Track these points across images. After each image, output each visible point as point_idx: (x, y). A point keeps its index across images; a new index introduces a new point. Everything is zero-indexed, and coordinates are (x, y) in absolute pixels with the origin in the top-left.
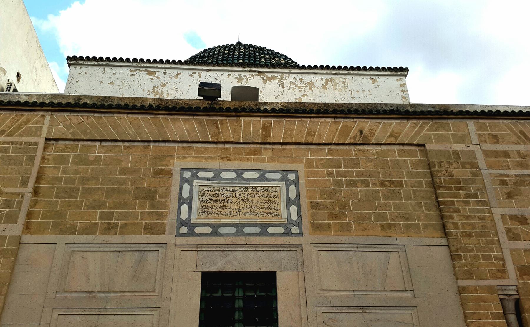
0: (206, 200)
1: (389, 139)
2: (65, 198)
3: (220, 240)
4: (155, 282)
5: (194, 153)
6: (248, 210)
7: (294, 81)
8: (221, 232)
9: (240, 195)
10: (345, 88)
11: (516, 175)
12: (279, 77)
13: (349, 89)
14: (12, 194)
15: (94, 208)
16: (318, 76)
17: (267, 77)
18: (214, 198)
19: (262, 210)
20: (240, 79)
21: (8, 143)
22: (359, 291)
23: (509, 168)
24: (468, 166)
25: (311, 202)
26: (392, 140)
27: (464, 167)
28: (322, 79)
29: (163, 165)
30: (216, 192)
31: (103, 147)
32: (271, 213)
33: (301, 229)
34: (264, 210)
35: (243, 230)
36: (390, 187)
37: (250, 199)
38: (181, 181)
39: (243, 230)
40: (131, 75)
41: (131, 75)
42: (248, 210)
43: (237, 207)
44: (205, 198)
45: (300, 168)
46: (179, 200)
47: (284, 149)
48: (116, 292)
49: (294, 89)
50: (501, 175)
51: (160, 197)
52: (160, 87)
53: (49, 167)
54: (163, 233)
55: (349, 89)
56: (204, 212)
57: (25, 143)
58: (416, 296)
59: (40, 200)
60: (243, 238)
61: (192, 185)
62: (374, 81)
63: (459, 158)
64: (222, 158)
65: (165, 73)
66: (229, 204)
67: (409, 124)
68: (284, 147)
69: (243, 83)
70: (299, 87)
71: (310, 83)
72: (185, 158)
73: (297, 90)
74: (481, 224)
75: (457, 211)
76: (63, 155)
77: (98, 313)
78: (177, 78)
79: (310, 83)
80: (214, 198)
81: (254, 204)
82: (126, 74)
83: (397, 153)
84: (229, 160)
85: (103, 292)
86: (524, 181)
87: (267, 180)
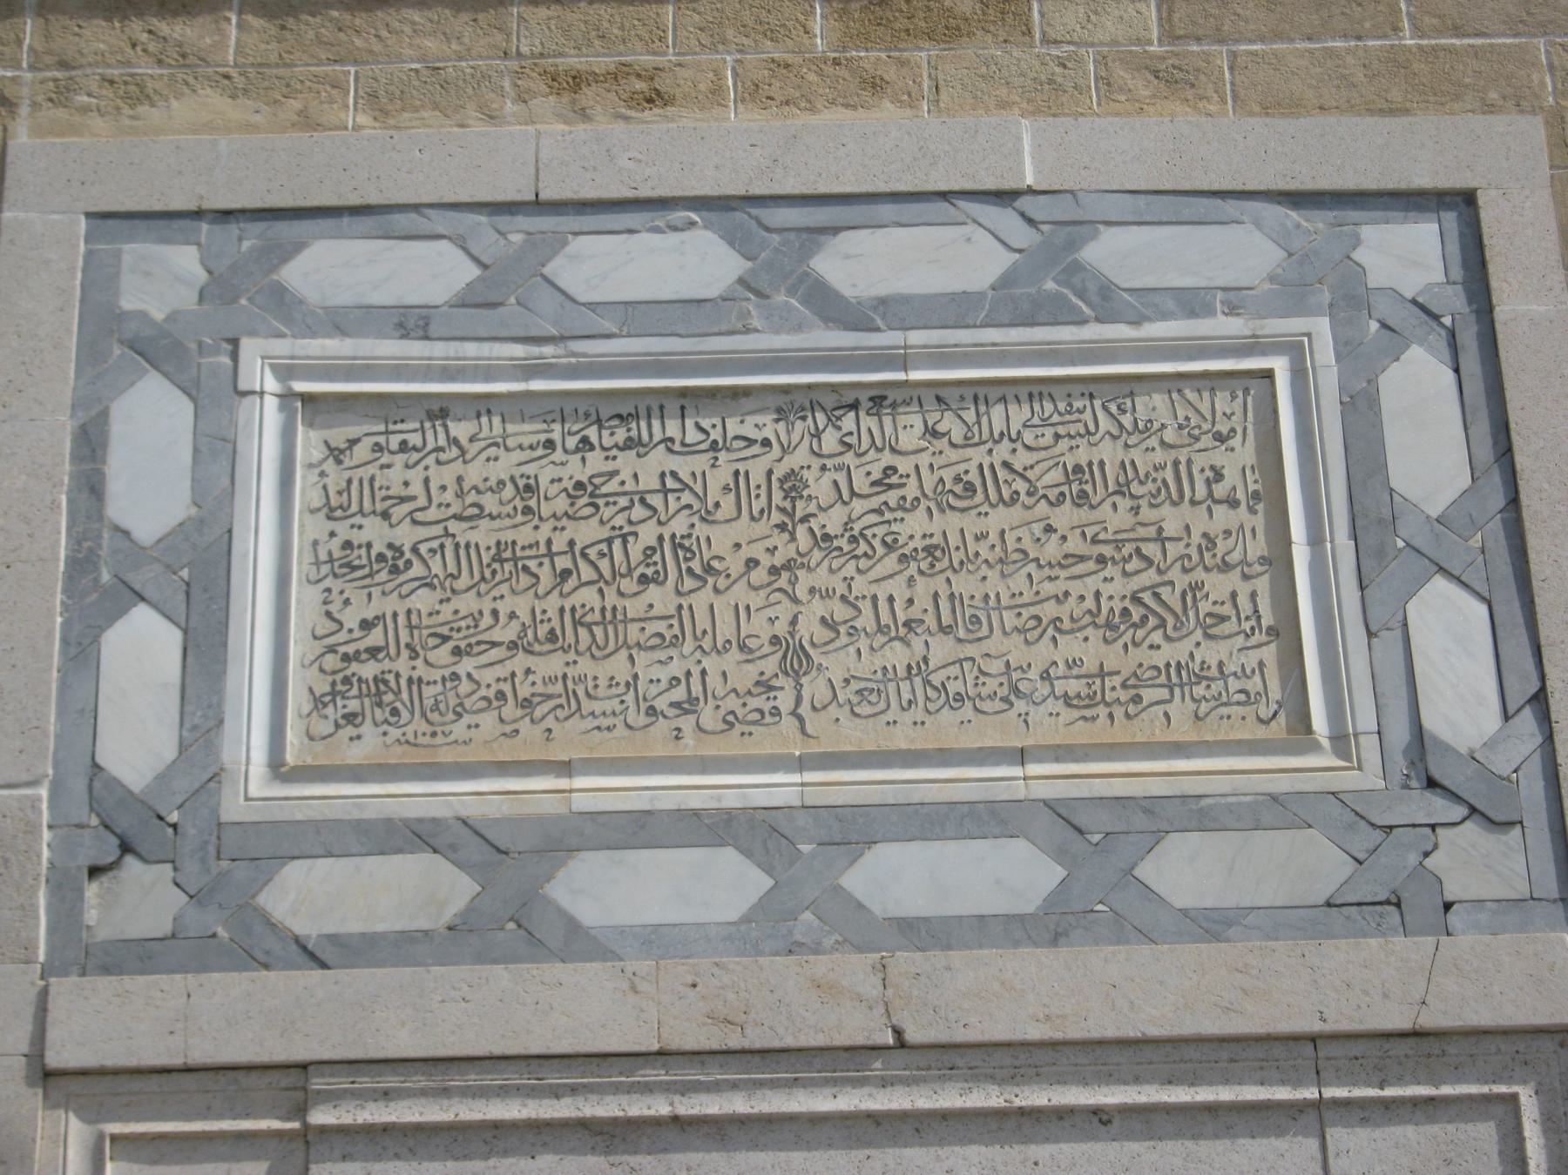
0: (394, 560)
6: (897, 656)
7: (335, 592)
8: (588, 914)
9: (793, 485)
18: (483, 535)
19: (1070, 647)
30: (506, 465)
32: (1180, 677)
34: (1090, 649)
35: (856, 880)
37: (914, 526)
38: (90, 354)
39: (856, 880)
42: (897, 656)
43: (758, 628)
44: (374, 532)
46: (81, 564)
60: (856, 971)
66: (660, 598)
80: (483, 535)
81: (964, 584)
84: (655, 99)
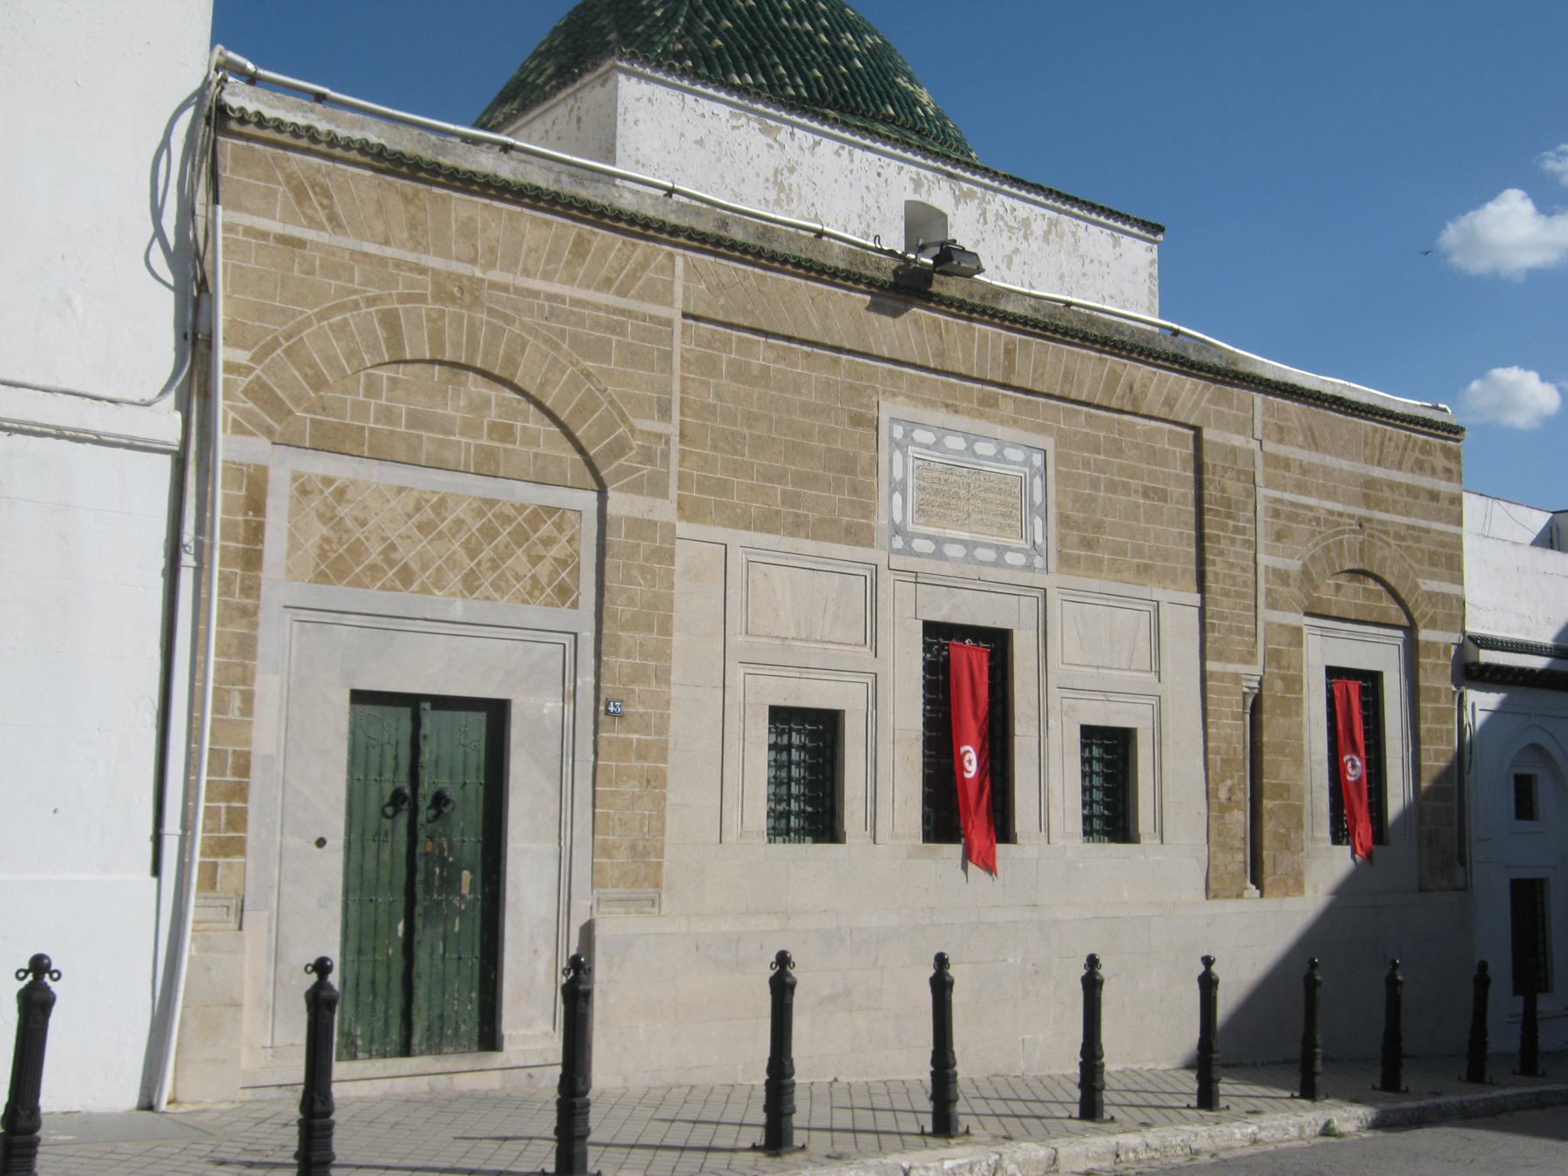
1: (1163, 410)
2: (727, 453)
3: (946, 568)
4: (289, 668)
5: (905, 385)
9: (969, 484)
10: (1075, 250)
11: (1292, 504)
12: (979, 195)
13: (1081, 251)
14: (649, 434)
15: (772, 481)
16: (1038, 210)
17: (961, 190)
20: (918, 184)
21: (622, 312)
22: (1103, 667)
23: (1285, 490)
24: (1243, 478)
25: (1061, 514)
26: (1164, 412)
27: (1238, 479)
28: (1044, 216)
29: (861, 405)
31: (771, 347)
33: (898, 552)
34: (1000, 519)
36: (1153, 499)
40: (734, 128)
41: (734, 128)
42: (980, 517)
45: (1048, 443)
47: (1029, 402)
48: (816, 641)
49: (1001, 231)
50: (1276, 500)
51: (864, 473)
52: (785, 172)
53: (693, 380)
54: (871, 545)
55: (1081, 251)
56: (923, 510)
57: (651, 318)
58: (225, 909)
59: (690, 452)
60: (975, 567)
61: (905, 455)
62: (1116, 243)
63: (1235, 462)
64: (947, 406)
65: (792, 134)
67: (1189, 382)
68: (1029, 397)
69: (922, 197)
70: (1010, 228)
71: (1026, 223)
72: (894, 395)
73: (1006, 234)
74: (1242, 579)
75: (1221, 553)
76: (710, 354)
77: (798, 675)
78: (813, 155)
79: (1026, 223)
82: (724, 121)
83: (1338, 507)
85: (801, 640)
86: (1297, 515)
87: (1006, 461)
